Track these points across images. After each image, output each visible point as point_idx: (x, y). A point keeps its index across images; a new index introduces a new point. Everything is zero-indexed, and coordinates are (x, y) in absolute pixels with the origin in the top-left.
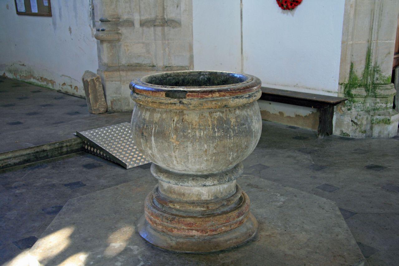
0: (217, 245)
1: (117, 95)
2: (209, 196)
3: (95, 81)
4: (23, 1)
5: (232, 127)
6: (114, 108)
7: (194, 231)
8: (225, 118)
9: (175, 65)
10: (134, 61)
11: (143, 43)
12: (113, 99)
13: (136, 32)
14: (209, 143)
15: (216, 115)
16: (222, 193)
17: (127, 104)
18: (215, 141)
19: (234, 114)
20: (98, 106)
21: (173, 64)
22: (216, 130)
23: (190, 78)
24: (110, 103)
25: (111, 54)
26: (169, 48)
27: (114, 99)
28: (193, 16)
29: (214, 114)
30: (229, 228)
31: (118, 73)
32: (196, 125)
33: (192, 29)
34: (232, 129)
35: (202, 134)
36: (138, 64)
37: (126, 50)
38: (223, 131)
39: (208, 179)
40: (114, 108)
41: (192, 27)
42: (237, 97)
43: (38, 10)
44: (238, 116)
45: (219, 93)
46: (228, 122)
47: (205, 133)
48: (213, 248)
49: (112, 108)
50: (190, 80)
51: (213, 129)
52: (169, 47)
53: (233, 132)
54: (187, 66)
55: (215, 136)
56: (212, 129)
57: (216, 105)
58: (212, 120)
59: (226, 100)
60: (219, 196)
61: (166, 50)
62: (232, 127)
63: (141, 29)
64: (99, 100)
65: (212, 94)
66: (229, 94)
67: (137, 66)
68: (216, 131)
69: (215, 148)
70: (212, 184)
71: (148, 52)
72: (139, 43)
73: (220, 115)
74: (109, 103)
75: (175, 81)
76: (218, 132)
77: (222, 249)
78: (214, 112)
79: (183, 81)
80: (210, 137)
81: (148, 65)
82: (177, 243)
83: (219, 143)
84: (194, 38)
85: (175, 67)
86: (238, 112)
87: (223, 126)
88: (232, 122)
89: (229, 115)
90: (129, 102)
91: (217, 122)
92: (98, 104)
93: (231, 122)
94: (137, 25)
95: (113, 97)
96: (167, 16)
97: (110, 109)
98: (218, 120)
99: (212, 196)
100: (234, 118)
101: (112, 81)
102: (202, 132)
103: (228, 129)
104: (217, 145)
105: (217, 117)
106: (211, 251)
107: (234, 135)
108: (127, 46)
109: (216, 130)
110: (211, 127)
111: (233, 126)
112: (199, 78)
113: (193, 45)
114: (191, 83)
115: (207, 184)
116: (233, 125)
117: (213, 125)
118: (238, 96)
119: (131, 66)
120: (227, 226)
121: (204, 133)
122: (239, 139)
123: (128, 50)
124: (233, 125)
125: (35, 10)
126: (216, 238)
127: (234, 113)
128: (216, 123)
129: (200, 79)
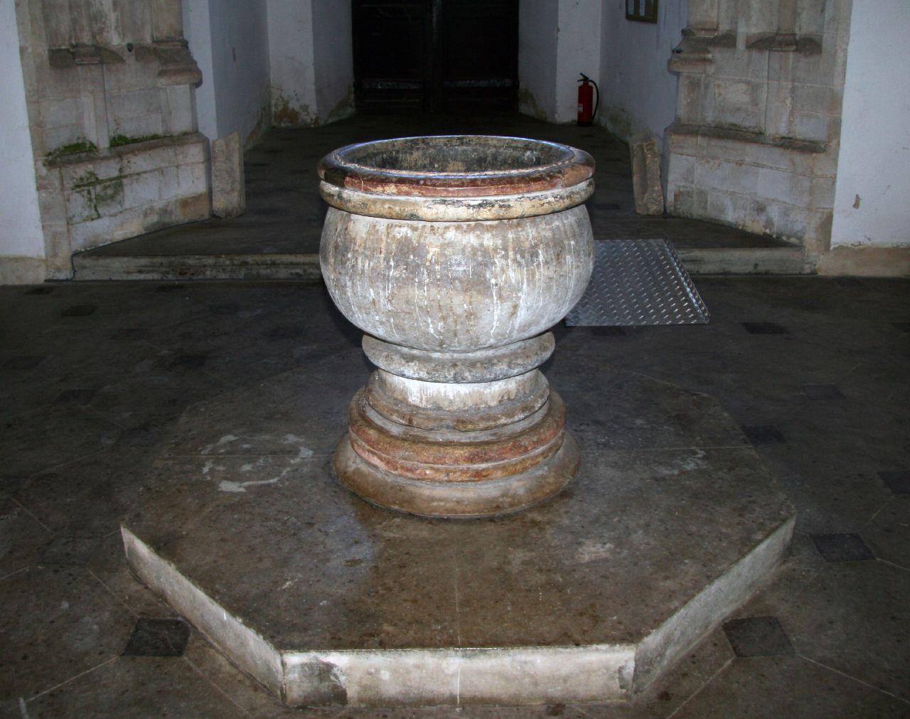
0: (411, 500)
1: (687, 184)
2: (421, 399)
3: (645, 151)
4: (633, 2)
5: (428, 264)
6: (679, 209)
7: (375, 458)
8: (415, 242)
9: (800, 135)
10: (729, 119)
11: (748, 83)
12: (680, 192)
13: (738, 59)
14: (378, 287)
15: (399, 233)
16: (451, 402)
17: (703, 204)
18: (388, 286)
19: (440, 237)
20: (645, 199)
21: (797, 134)
22: (392, 263)
23: (509, 154)
24: (673, 197)
25: (689, 100)
26: (793, 99)
27: (681, 190)
28: (851, 33)
29: (397, 229)
30: (443, 477)
31: (694, 140)
32: (360, 246)
33: (845, 63)
34: (427, 268)
35: (367, 265)
36: (735, 125)
37: (717, 95)
38: (406, 269)
39: (410, 364)
40: (679, 209)
41: (846, 56)
42: (444, 202)
43: (646, 12)
44: (449, 243)
45: (396, 186)
46: (419, 250)
47: (371, 264)
48: (397, 502)
49: (675, 209)
50: (509, 157)
51: (387, 260)
52: (793, 95)
53: (428, 275)
54: (824, 142)
55: (389, 276)
56: (384, 260)
57: (390, 210)
58: (389, 241)
59: (415, 204)
60: (445, 405)
61: (787, 102)
62: (428, 264)
63: (746, 54)
64: (650, 189)
65: (383, 187)
66: (419, 193)
67: (731, 129)
68: (391, 266)
69: (390, 301)
70: (416, 376)
71: (755, 102)
72: (740, 81)
73: (407, 234)
74: (670, 198)
75: (478, 155)
76: (396, 267)
77: (413, 512)
78: (396, 226)
79: (495, 157)
80: (378, 274)
81: (751, 130)
82: (357, 471)
83: (395, 292)
84: (846, 81)
85: (799, 140)
86: (451, 235)
87: (408, 258)
88: (431, 254)
89: (426, 237)
90: (707, 202)
91: (397, 248)
92: (646, 196)
93: (428, 252)
94: (741, 44)
95: (680, 187)
96: (800, 29)
97: (672, 209)
98: (399, 242)
99: (427, 401)
100: (436, 247)
101: (682, 155)
102: (367, 261)
103: (418, 266)
104: (393, 295)
105: (399, 236)
106: (392, 506)
107: (432, 283)
108: (719, 86)
109: (392, 263)
110: (382, 255)
111: (430, 262)
112: (524, 155)
113: (841, 99)
114: (509, 164)
115: (406, 372)
116: (431, 259)
117: (389, 253)
118: (448, 199)
119: (720, 128)
120: (437, 470)
121: (369, 264)
122: (442, 293)
123: (720, 94)
124: (431, 259)
125: (642, 13)
126: (417, 487)
127: (442, 235)
128: (394, 247)
129: (526, 159)
